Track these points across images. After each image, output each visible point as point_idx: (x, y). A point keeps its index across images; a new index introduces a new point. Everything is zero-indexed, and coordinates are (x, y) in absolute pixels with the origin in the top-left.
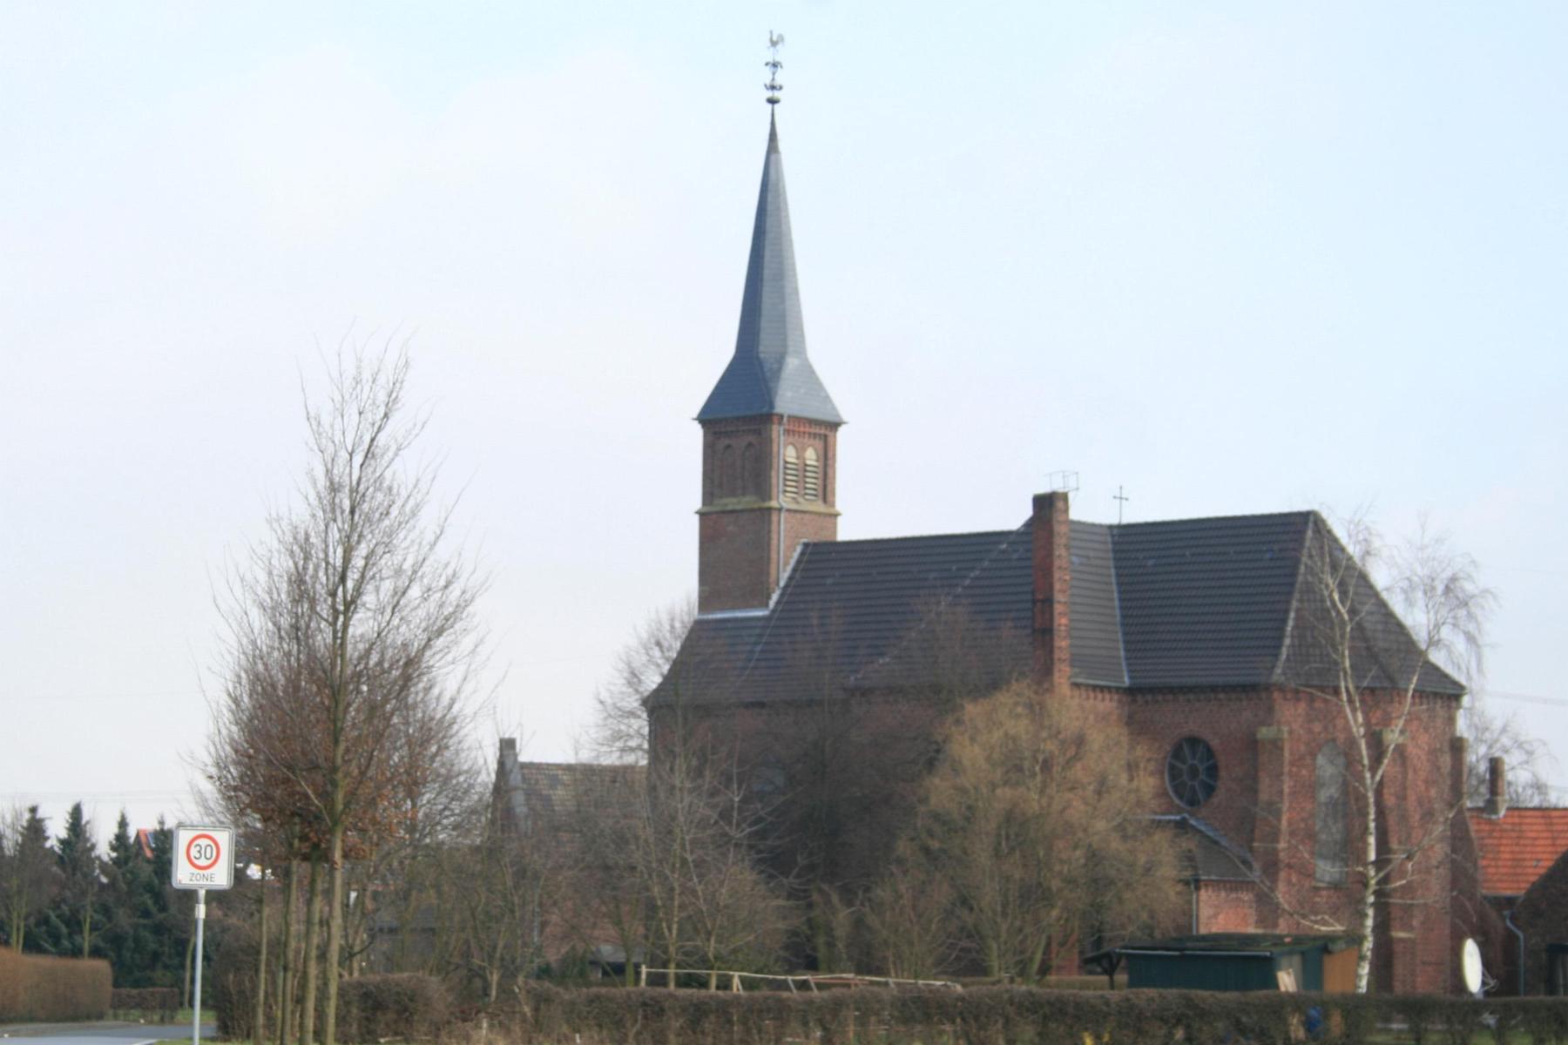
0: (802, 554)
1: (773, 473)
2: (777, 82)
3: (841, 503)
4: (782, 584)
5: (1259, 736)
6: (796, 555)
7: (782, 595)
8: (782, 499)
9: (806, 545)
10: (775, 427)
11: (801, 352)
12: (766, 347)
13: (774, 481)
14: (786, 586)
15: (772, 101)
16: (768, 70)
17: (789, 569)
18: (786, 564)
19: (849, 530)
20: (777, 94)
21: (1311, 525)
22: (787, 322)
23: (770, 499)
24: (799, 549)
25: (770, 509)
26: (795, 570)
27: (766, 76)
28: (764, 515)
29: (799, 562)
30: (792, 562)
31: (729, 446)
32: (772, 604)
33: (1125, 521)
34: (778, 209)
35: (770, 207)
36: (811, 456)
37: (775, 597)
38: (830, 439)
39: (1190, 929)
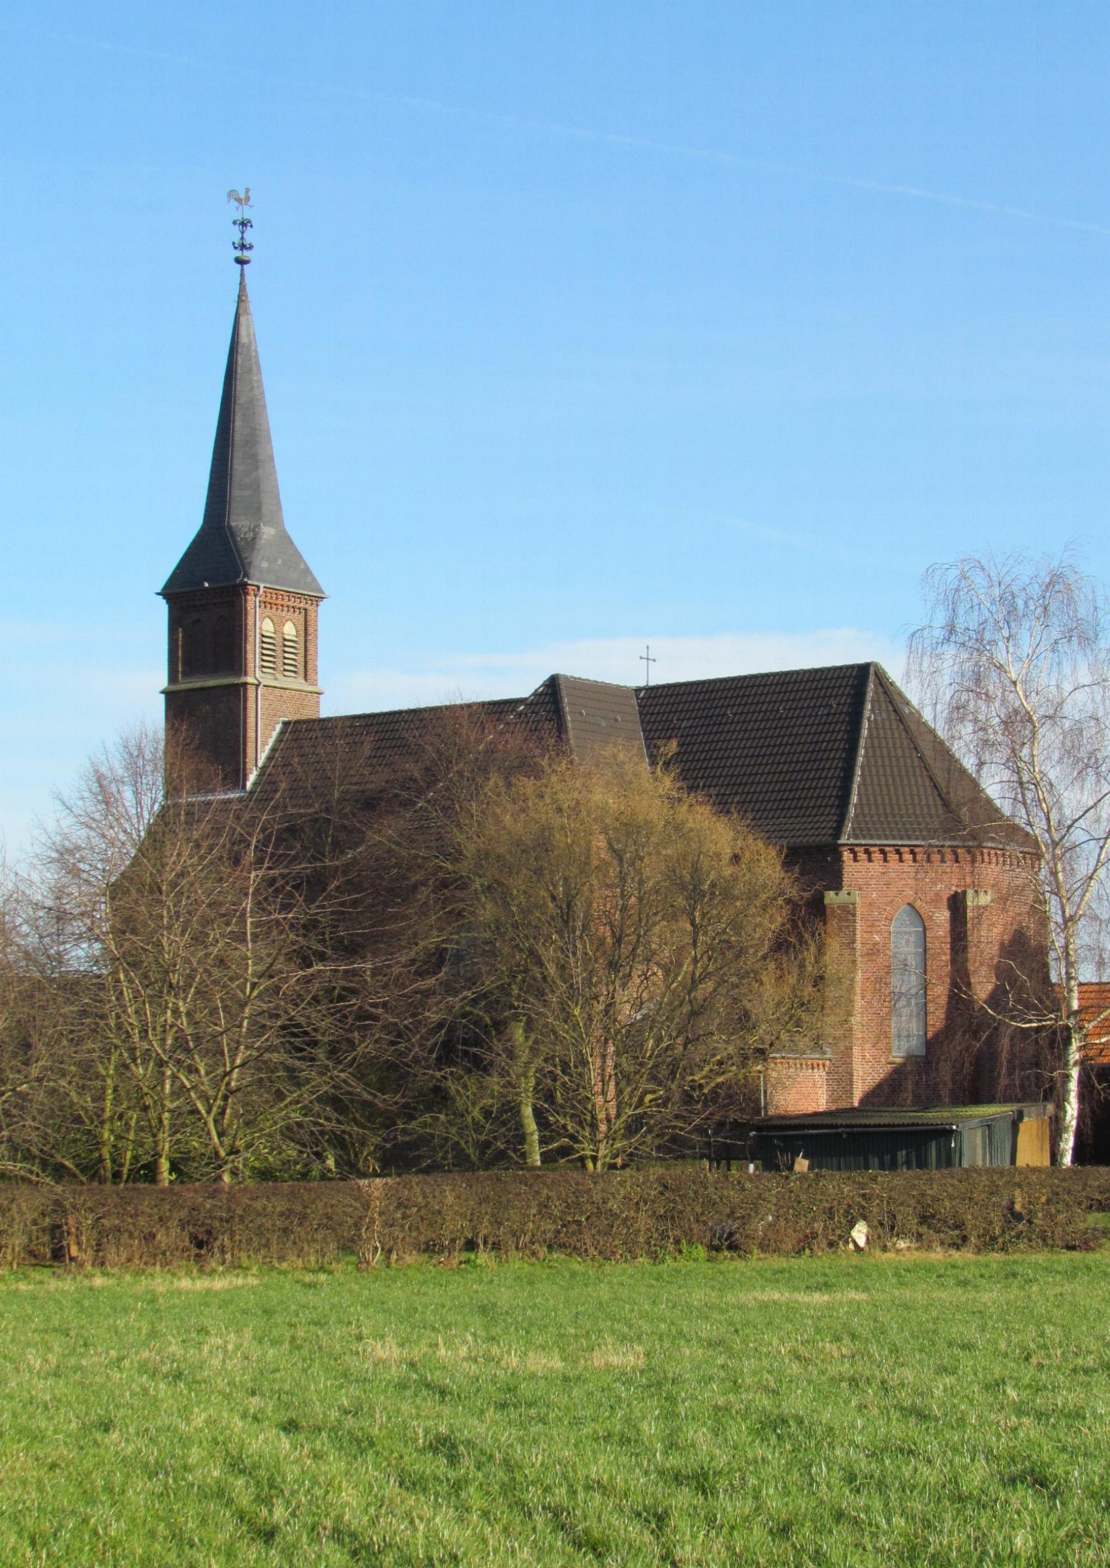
0: (282, 733)
1: (249, 647)
2: (247, 242)
3: (322, 685)
4: (260, 764)
5: (826, 901)
6: (275, 734)
7: (260, 776)
8: (256, 674)
9: (286, 724)
10: (250, 598)
11: (277, 522)
12: (239, 522)
13: (250, 656)
14: (264, 767)
15: (241, 262)
16: (237, 229)
17: (267, 749)
18: (265, 744)
19: (328, 710)
20: (247, 254)
21: (872, 677)
22: (263, 503)
23: (246, 674)
24: (279, 727)
25: (246, 684)
26: (274, 750)
27: (235, 234)
28: (237, 693)
29: (279, 740)
30: (271, 742)
31: (198, 621)
32: (249, 785)
33: (652, 683)
34: (256, 487)
35: (242, 398)
36: (289, 630)
37: (252, 778)
38: (311, 614)
39: (757, 1111)
